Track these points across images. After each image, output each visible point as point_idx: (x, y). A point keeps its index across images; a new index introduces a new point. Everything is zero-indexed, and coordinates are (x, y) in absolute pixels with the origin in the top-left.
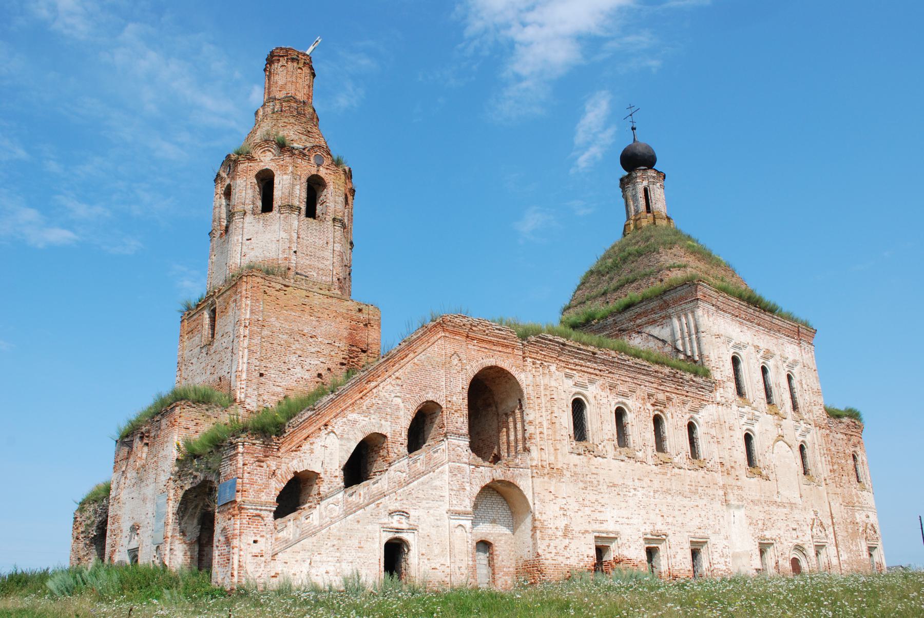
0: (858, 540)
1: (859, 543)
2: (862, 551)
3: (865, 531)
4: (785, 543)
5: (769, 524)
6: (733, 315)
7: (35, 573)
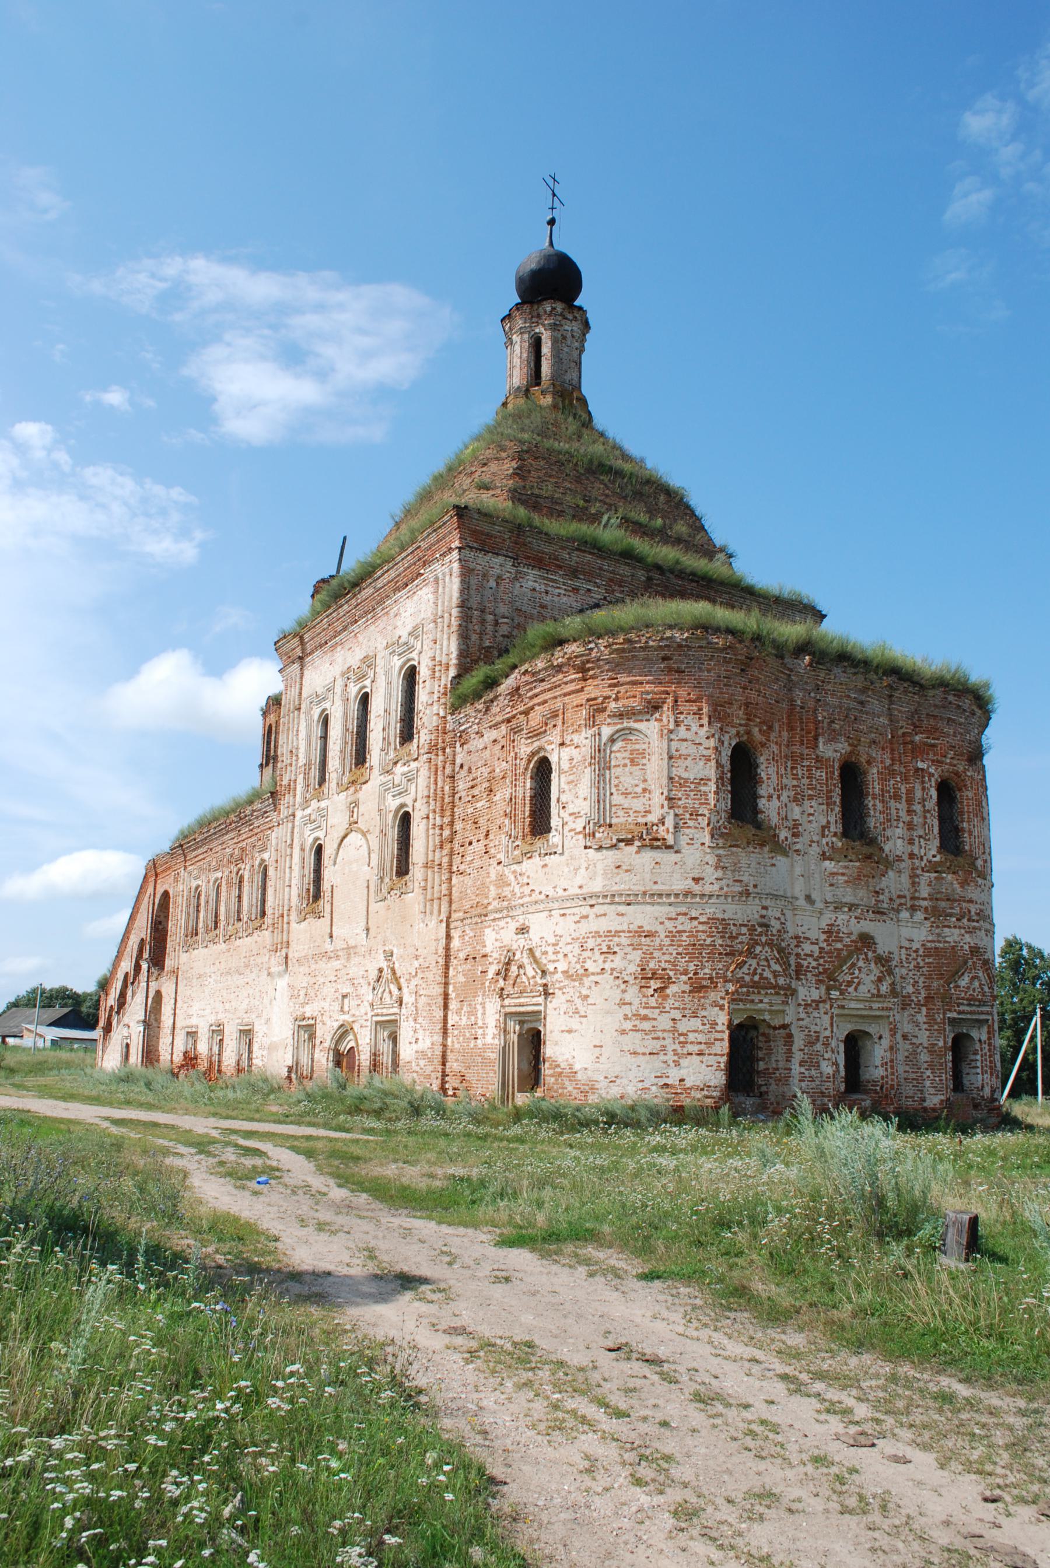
0: (480, 999)
1: (479, 1007)
2: (485, 1026)
3: (504, 972)
4: (329, 1023)
5: (312, 994)
6: (321, 646)
7: (832, 642)
